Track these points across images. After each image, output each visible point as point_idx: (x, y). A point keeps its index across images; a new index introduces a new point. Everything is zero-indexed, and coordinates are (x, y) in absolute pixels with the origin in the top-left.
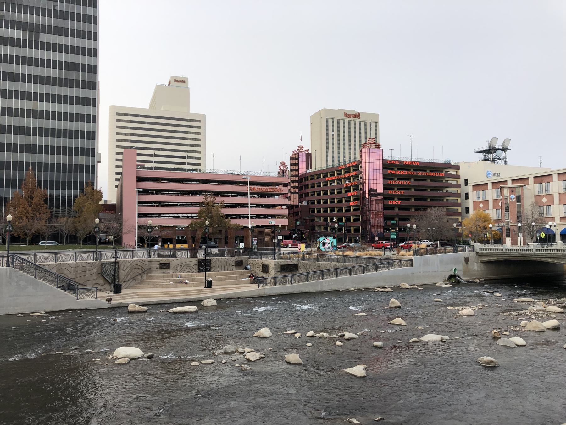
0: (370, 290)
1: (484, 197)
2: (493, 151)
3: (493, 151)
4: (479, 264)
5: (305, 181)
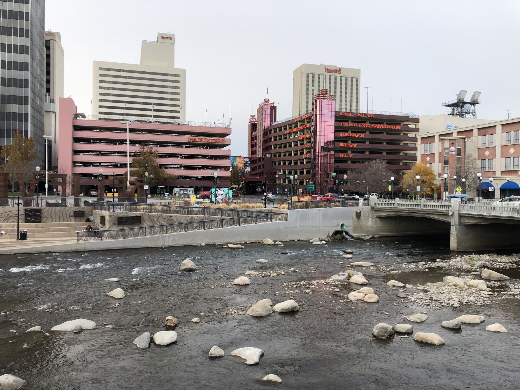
0: (220, 247)
1: (431, 150)
2: (461, 105)
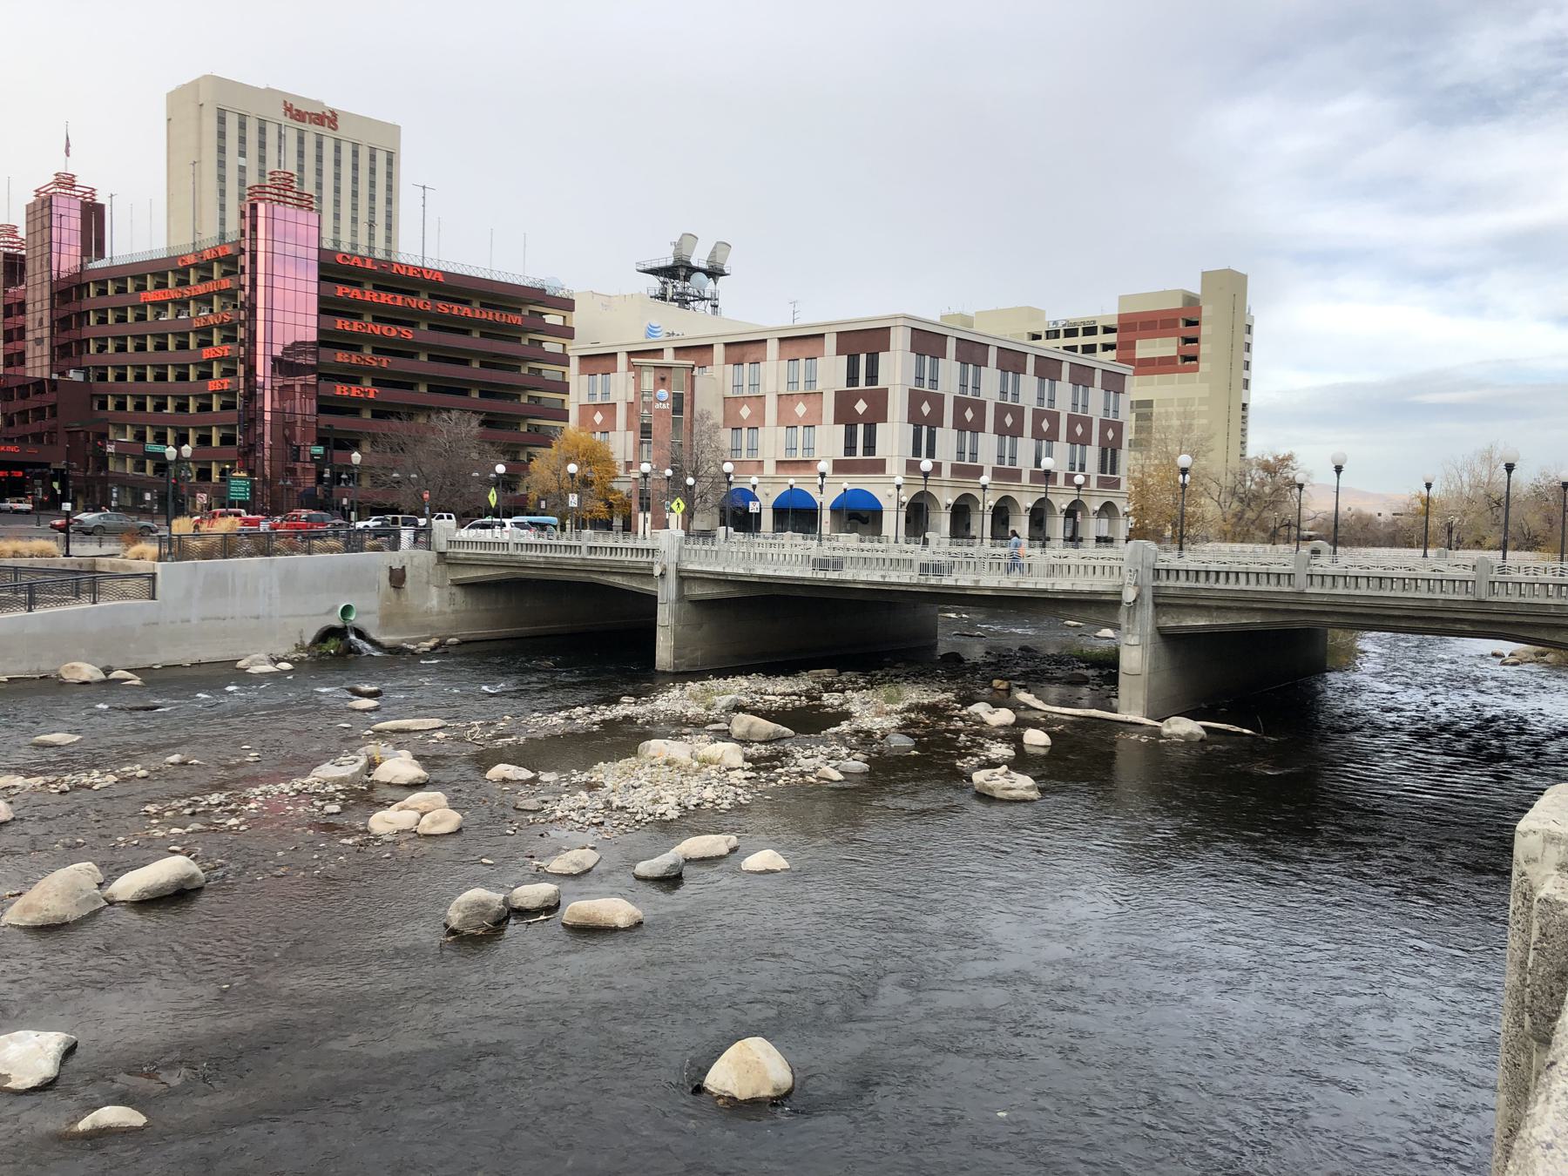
1: (606, 394)
2: (682, 273)
3: (682, 273)
4: (446, 593)
5: (80, 297)
